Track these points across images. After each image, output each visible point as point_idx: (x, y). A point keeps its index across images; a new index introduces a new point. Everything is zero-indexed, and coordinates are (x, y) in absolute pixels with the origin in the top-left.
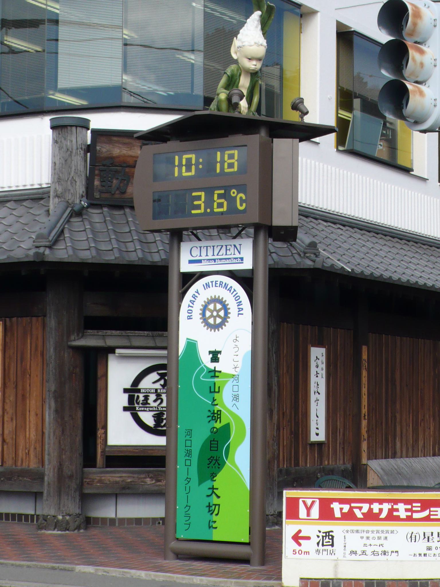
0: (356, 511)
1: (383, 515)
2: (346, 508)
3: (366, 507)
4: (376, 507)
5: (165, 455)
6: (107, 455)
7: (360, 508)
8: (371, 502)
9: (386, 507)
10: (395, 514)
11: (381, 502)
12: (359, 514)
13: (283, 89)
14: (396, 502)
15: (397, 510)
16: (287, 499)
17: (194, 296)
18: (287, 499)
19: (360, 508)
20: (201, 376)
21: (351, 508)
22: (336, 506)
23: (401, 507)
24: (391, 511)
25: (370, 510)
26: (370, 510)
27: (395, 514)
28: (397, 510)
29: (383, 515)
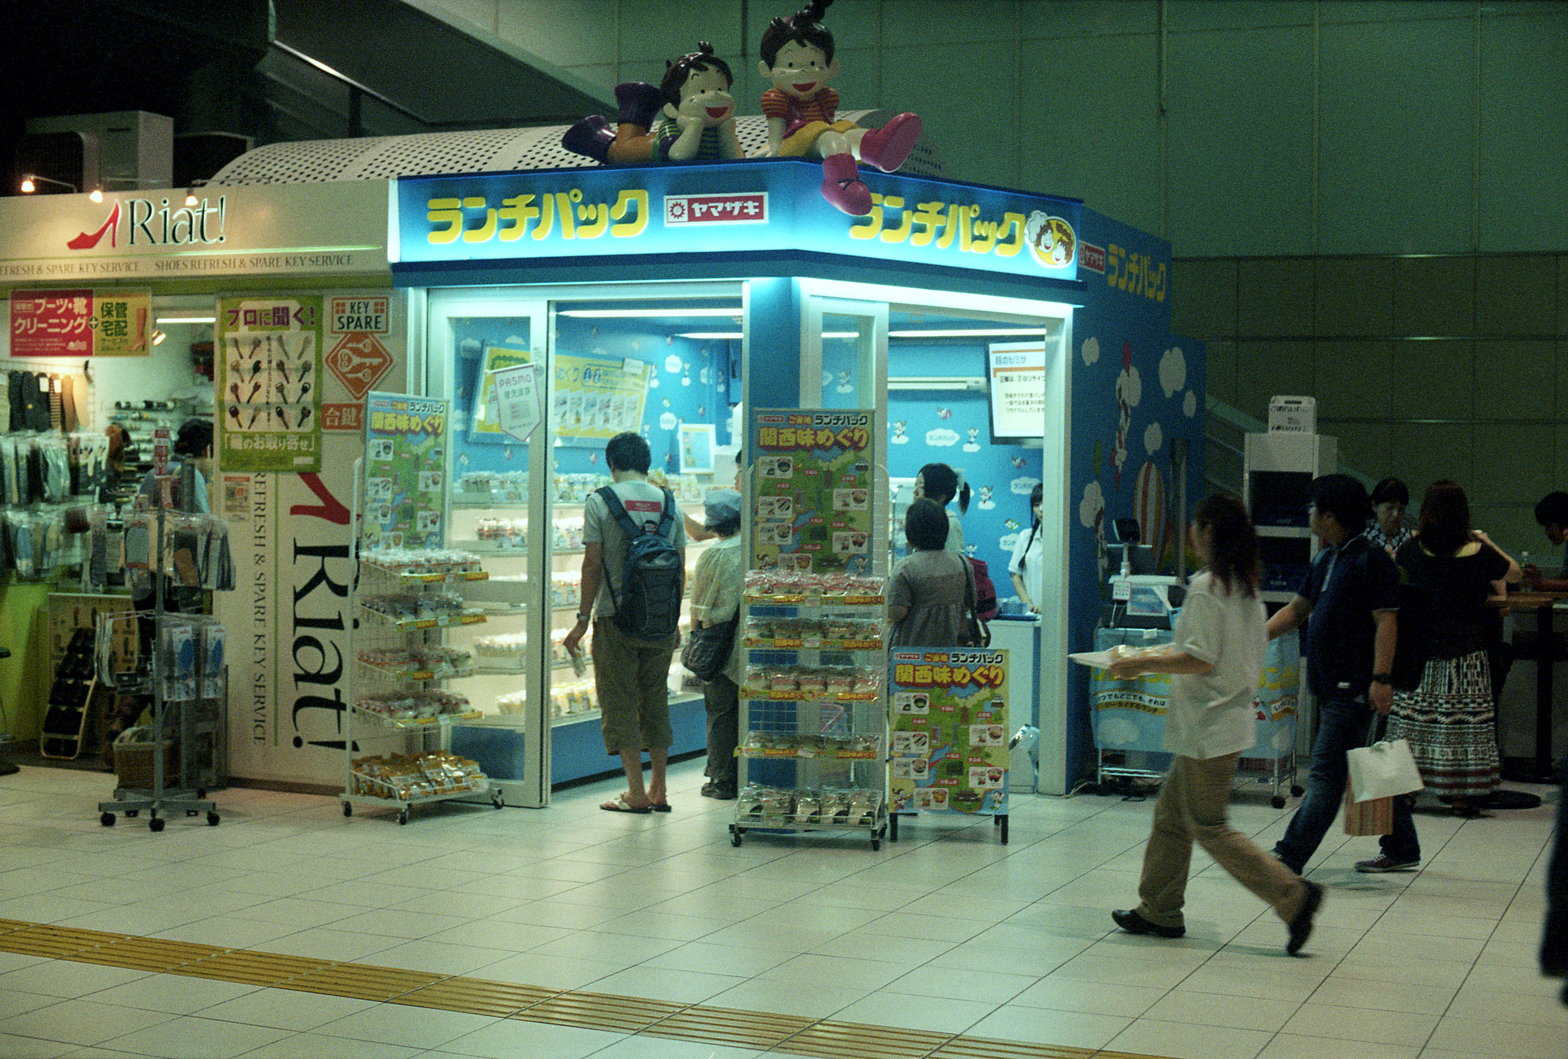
0: (713, 210)
1: (736, 212)
2: (704, 207)
3: (720, 206)
4: (729, 206)
5: (1167, 588)
6: (554, 726)
7: (716, 207)
8: (725, 200)
9: (738, 205)
10: (745, 211)
11: (733, 200)
12: (716, 214)
13: (413, 973)
14: (746, 199)
15: (747, 208)
16: (1253, 474)
17: (262, 610)
18: (1253, 474)
19: (716, 207)
20: (266, 31)
21: (709, 208)
22: (696, 206)
23: (750, 204)
24: (742, 208)
25: (725, 208)
26: (725, 208)
27: (745, 211)
28: (747, 208)
29: (736, 212)
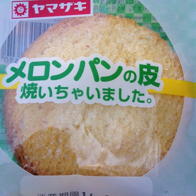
2: (42, 7)
7: (52, 7)
19: (52, 7)
21: (46, 8)
